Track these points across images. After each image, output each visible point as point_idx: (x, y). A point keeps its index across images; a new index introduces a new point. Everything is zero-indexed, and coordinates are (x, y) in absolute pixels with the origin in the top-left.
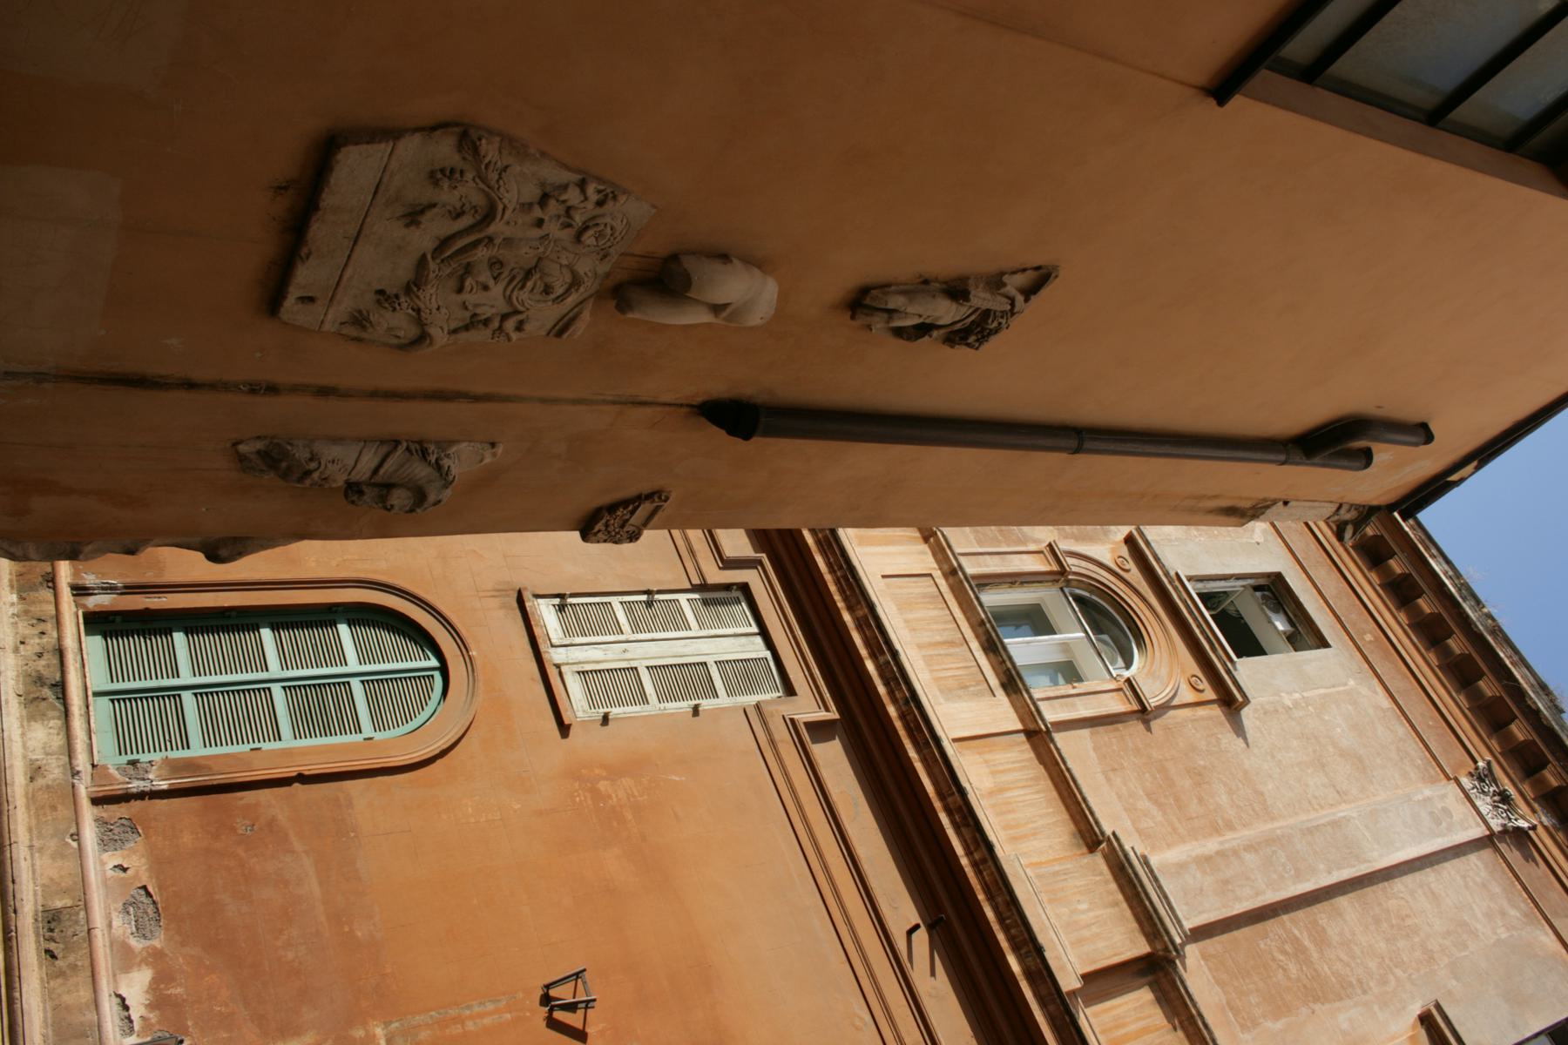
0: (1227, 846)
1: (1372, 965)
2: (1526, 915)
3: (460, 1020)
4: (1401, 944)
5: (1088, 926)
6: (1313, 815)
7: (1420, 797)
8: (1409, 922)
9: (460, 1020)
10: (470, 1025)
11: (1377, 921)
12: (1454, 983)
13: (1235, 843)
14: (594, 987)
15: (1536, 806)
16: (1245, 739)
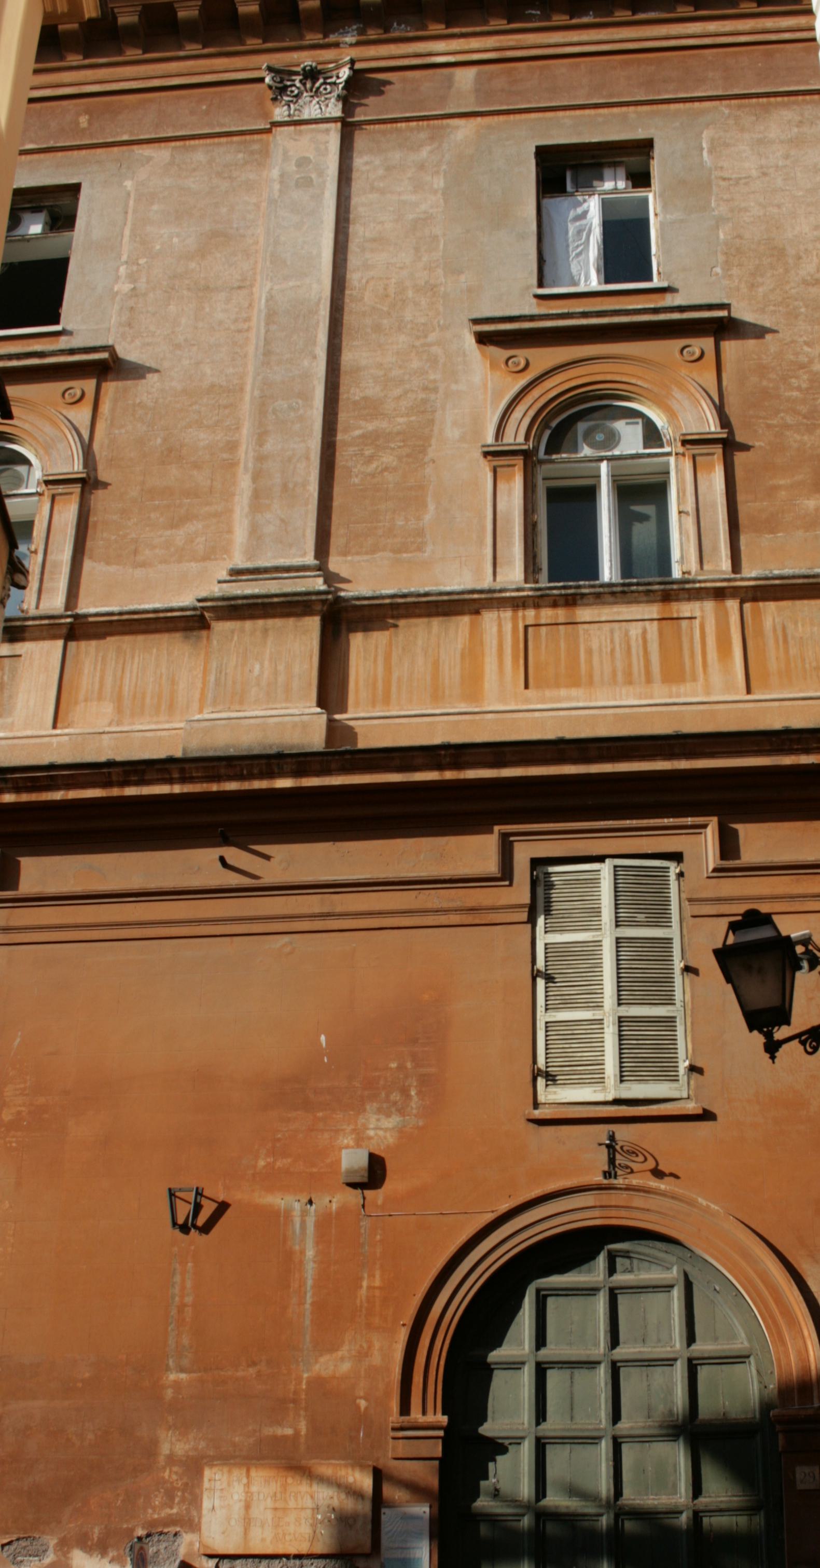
0: (250, 465)
1: (415, 364)
2: (432, 139)
3: (181, 1308)
4: (408, 316)
5: (276, 673)
6: (252, 335)
7: (277, 186)
8: (392, 290)
9: (181, 1308)
10: (189, 1300)
11: (377, 328)
12: (463, 278)
13: (251, 454)
14: (188, 1181)
15: (332, 38)
16: (150, 370)
